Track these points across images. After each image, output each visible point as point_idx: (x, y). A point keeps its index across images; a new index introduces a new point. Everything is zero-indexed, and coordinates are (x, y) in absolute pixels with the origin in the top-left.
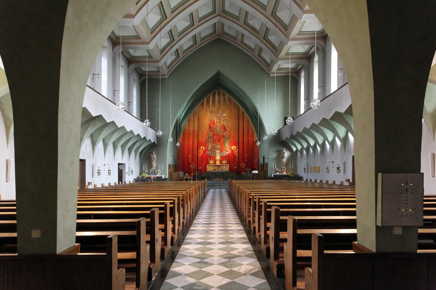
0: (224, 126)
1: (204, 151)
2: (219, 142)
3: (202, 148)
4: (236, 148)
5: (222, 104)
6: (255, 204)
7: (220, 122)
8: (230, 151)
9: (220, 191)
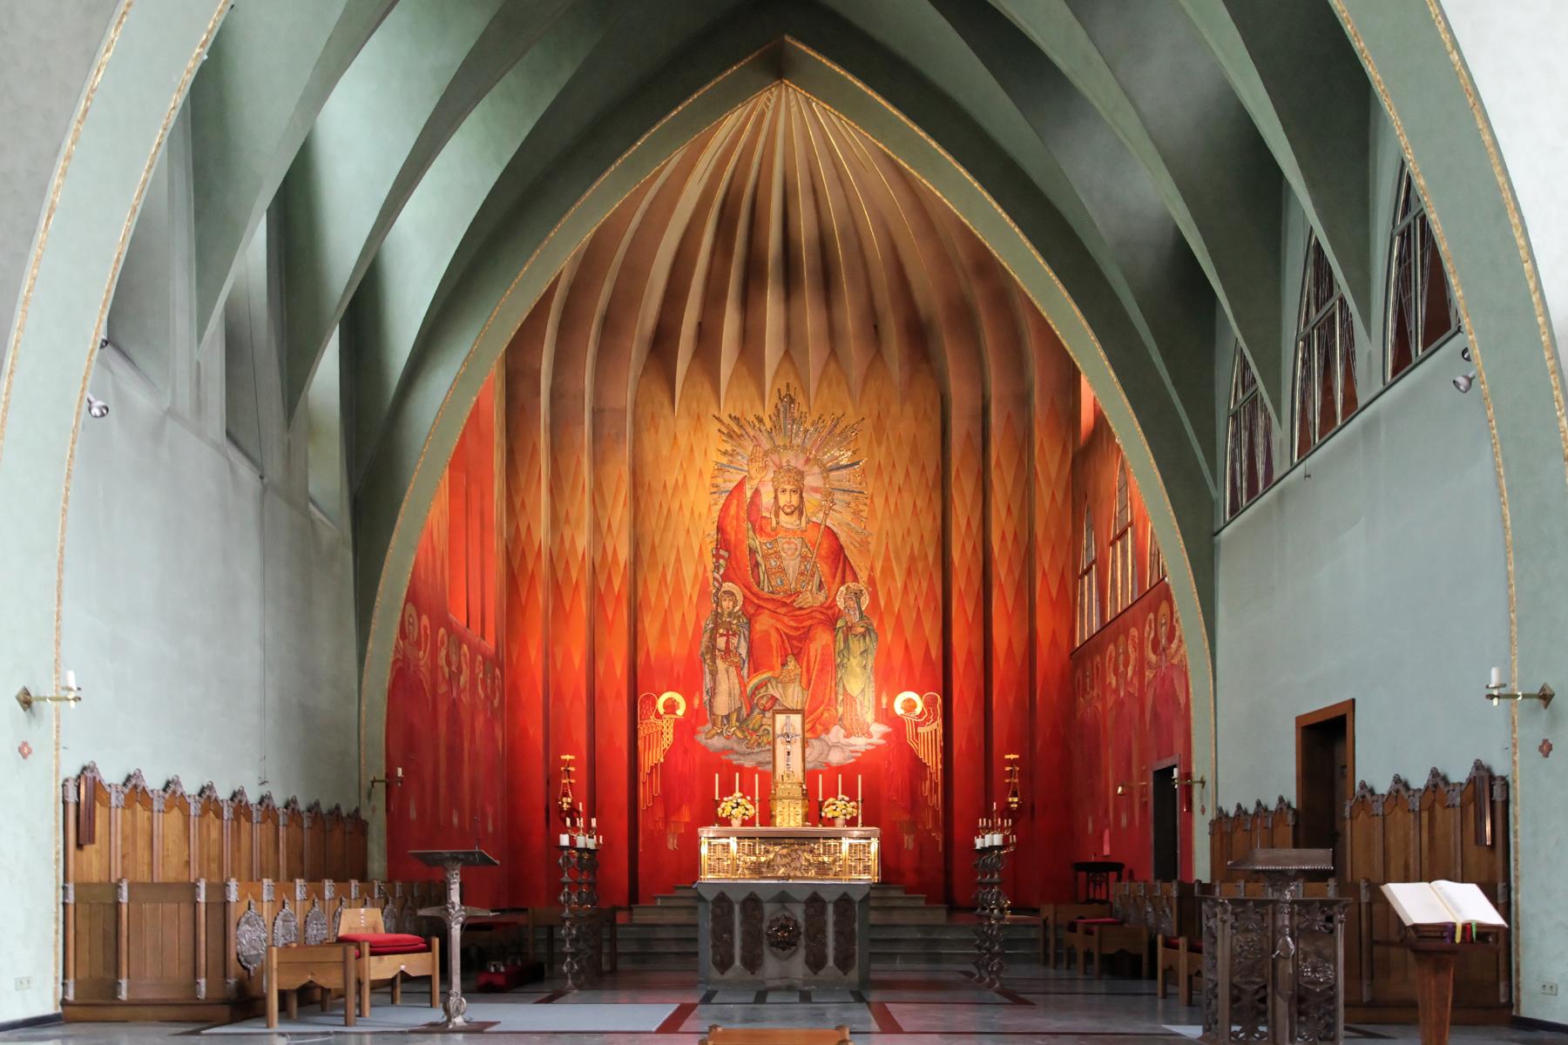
1: (678, 724)
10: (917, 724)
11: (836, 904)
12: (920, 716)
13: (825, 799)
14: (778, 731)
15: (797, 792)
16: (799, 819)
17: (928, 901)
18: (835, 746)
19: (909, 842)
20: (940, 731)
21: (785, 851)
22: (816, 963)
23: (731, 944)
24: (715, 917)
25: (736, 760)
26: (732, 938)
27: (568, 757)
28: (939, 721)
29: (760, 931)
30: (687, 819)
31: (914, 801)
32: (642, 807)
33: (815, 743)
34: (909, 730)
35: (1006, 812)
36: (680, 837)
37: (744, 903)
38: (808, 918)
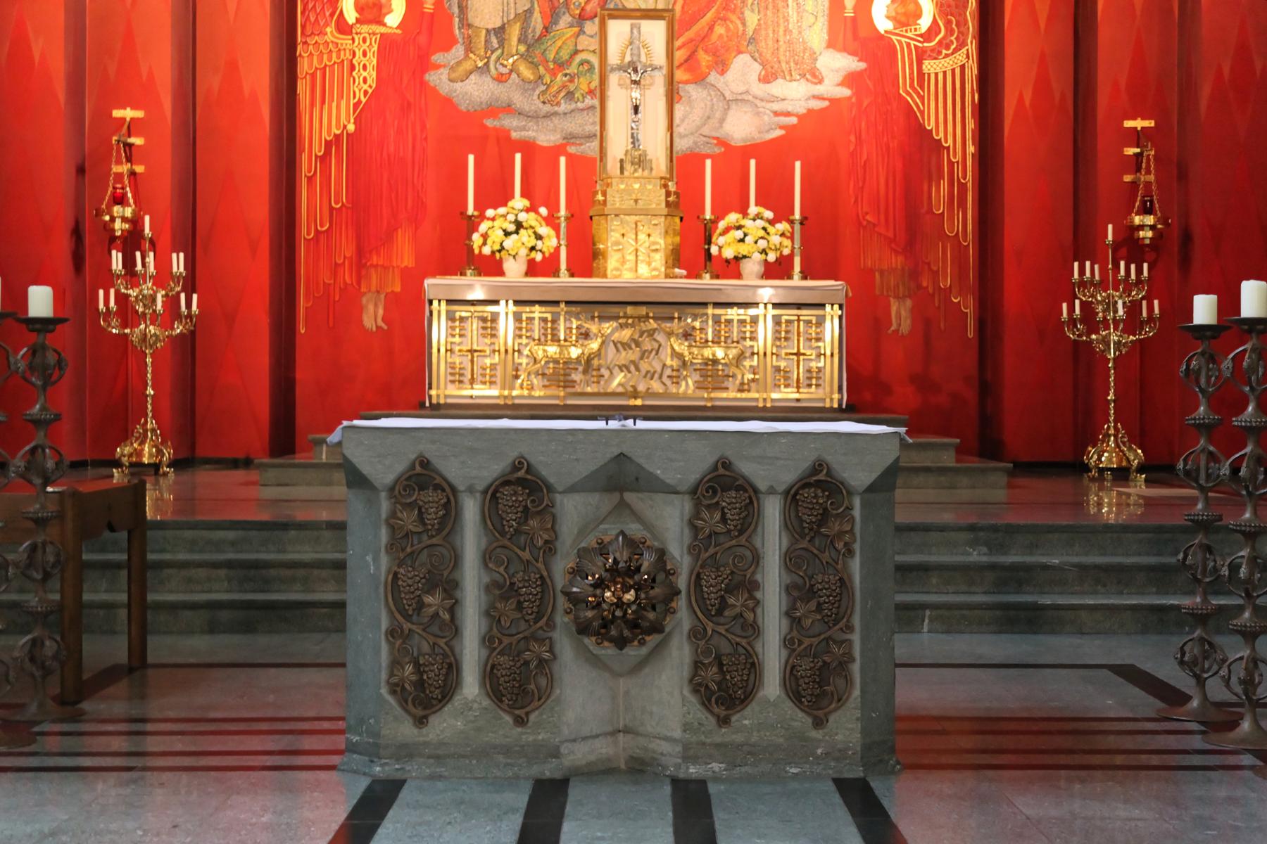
1: (387, 46)
10: (921, 55)
11: (792, 497)
12: (928, 36)
13: (719, 214)
14: (613, 58)
15: (656, 198)
16: (659, 260)
17: (961, 451)
18: (739, 100)
19: (901, 315)
20: (973, 70)
21: (626, 334)
22: (724, 688)
23: (453, 628)
24: (399, 541)
25: (518, 129)
26: (454, 608)
27: (128, 114)
28: (972, 46)
29: (544, 583)
30: (408, 261)
31: (914, 228)
32: (305, 232)
33: (692, 91)
34: (905, 68)
35: (1130, 247)
36: (393, 302)
37: (492, 496)
38: (701, 541)
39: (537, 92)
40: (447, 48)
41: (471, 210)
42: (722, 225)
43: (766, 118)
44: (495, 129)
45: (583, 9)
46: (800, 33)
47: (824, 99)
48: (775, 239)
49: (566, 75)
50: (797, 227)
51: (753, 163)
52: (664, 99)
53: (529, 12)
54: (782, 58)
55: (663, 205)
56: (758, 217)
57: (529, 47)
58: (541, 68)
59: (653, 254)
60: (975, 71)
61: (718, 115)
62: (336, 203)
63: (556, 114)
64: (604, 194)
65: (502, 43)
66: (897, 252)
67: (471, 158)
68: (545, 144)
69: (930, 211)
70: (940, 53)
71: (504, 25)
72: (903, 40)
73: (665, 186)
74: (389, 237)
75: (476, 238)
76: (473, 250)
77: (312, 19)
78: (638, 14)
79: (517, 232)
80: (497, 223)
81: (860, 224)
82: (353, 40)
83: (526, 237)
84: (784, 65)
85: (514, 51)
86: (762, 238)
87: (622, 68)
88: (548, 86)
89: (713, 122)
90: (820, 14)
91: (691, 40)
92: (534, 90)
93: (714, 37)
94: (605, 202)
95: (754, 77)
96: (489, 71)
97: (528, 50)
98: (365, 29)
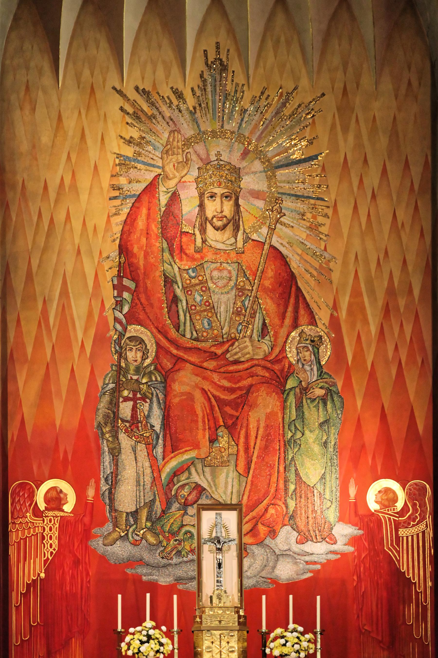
0: (277, 255)
1: (65, 524)
2: (232, 429)
3: (55, 500)
4: (414, 496)
5: (254, 27)
6: (164, 459)
7: (234, 223)
8: (344, 532)
9: (195, 578)
10: (398, 526)
12: (402, 513)
13: (271, 629)
14: (205, 534)
15: (231, 619)
25: (146, 575)
34: (387, 533)
39: (158, 551)
40: (102, 524)
41: (120, 628)
42: (272, 635)
43: (301, 566)
44: (133, 575)
45: (186, 499)
46: (322, 512)
47: (337, 553)
48: (305, 644)
49: (176, 540)
50: (319, 636)
51: (291, 597)
52: (237, 558)
53: (153, 501)
54: (311, 528)
55: (237, 624)
56: (294, 630)
57: (153, 523)
58: (161, 536)
59: (230, 654)
60: (431, 535)
61: (271, 564)
62: (34, 623)
63: (170, 565)
64: (201, 618)
65: (136, 522)
66: (383, 649)
67: (120, 596)
68: (163, 584)
69: (404, 623)
70: (409, 524)
71: (137, 509)
72: (386, 516)
73: (238, 612)
74: (66, 644)
75: (124, 646)
76: (122, 653)
77: (18, 508)
78: (220, 507)
79: (148, 642)
80: (136, 636)
81: (361, 631)
82: (43, 521)
83: (153, 644)
84: (312, 532)
85: (144, 527)
86: (297, 643)
87: (211, 540)
88: (165, 547)
89: (268, 569)
90: (334, 500)
91: (254, 518)
92: (156, 550)
93: (268, 515)
94: (201, 622)
95: (293, 540)
96: (128, 539)
97: (152, 525)
98: (51, 513)
